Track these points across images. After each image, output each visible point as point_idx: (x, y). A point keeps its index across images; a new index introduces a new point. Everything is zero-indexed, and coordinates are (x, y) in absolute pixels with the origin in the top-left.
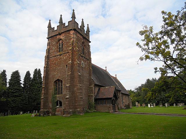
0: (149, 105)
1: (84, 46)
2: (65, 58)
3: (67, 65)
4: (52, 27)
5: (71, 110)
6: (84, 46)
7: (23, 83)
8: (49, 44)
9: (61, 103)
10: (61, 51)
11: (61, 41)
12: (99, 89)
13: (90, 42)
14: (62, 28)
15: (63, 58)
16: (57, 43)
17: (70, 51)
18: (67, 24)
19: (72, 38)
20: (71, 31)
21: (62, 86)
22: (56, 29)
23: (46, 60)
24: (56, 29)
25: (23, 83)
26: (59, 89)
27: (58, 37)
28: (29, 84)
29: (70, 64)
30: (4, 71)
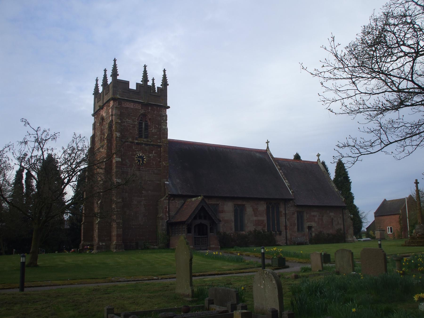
5: (104, 244)
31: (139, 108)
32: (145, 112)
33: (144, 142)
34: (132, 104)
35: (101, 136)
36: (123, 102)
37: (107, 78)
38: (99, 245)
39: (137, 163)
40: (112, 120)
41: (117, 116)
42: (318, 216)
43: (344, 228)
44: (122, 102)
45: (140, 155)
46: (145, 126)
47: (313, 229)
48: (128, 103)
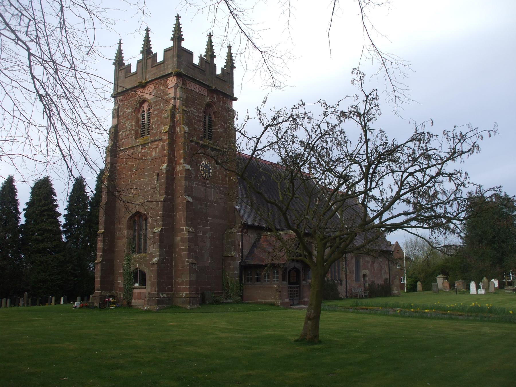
0: (473, 285)
1: (213, 115)
2: (154, 154)
3: (158, 175)
4: (126, 63)
5: (165, 296)
6: (213, 115)
7: (66, 212)
8: (117, 114)
9: (144, 276)
10: (146, 132)
11: (146, 106)
12: (259, 239)
13: (236, 99)
14: (149, 68)
15: (151, 154)
16: (137, 110)
17: (165, 138)
18: (160, 58)
19: (170, 99)
20: (170, 79)
21: (146, 229)
22: (133, 69)
23: (109, 159)
24: (133, 69)
25: (66, 212)
26: (140, 239)
27: (139, 93)
28: (82, 216)
29: (164, 172)
30: (10, 181)
31: (204, 94)
32: (210, 101)
33: (210, 145)
34: (197, 86)
35: (137, 128)
36: (188, 82)
37: (150, 42)
38: (160, 298)
39: (203, 174)
40: (174, 106)
41: (182, 101)
42: (370, 261)
43: (389, 278)
44: (187, 80)
45: (205, 163)
46: (209, 122)
47: (367, 279)
48: (193, 84)
